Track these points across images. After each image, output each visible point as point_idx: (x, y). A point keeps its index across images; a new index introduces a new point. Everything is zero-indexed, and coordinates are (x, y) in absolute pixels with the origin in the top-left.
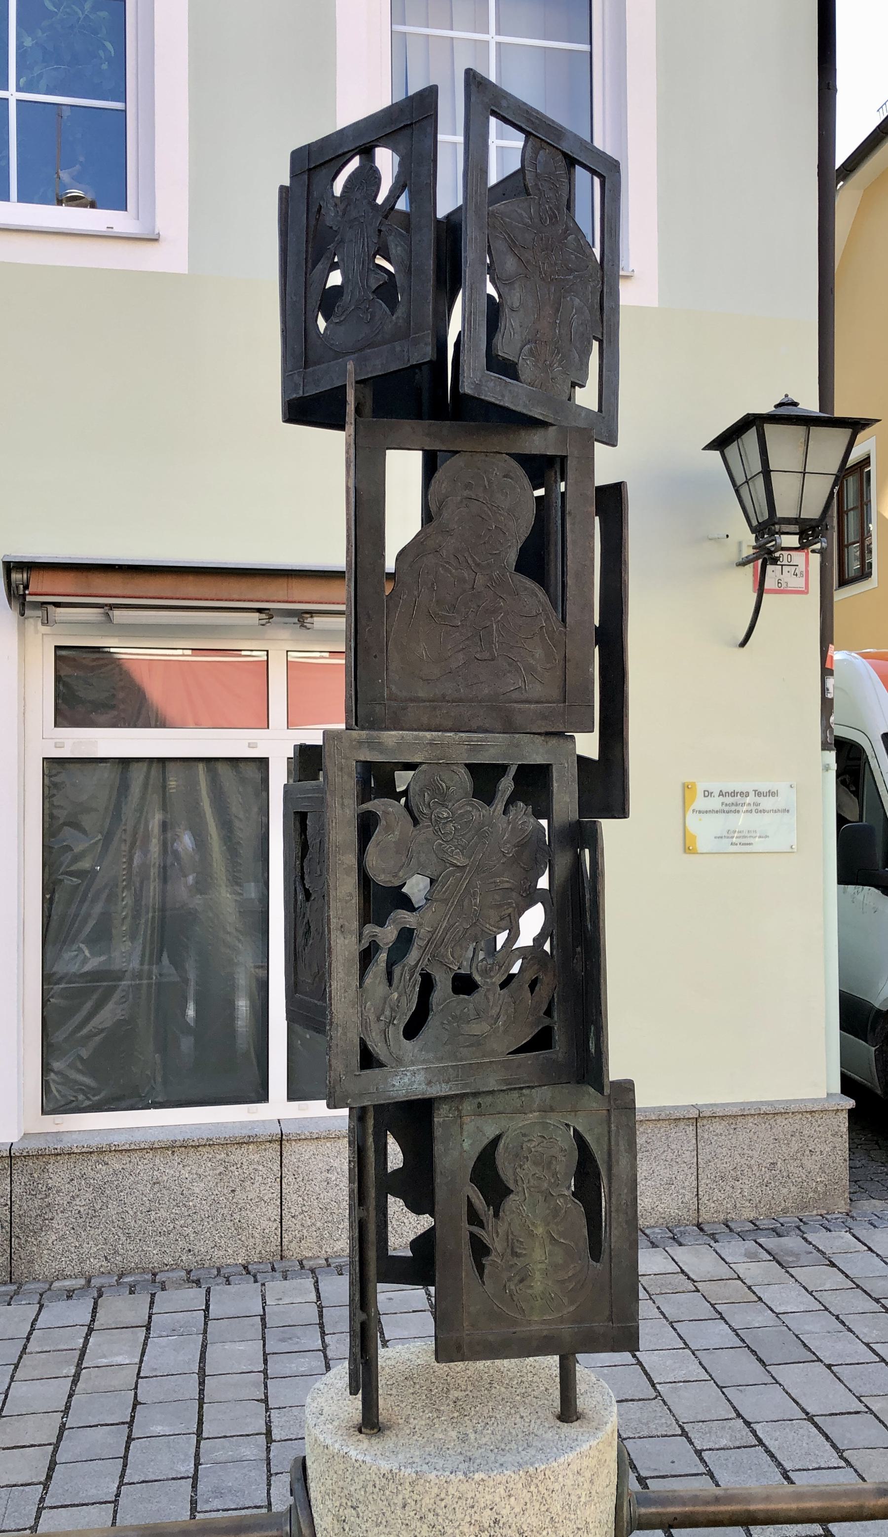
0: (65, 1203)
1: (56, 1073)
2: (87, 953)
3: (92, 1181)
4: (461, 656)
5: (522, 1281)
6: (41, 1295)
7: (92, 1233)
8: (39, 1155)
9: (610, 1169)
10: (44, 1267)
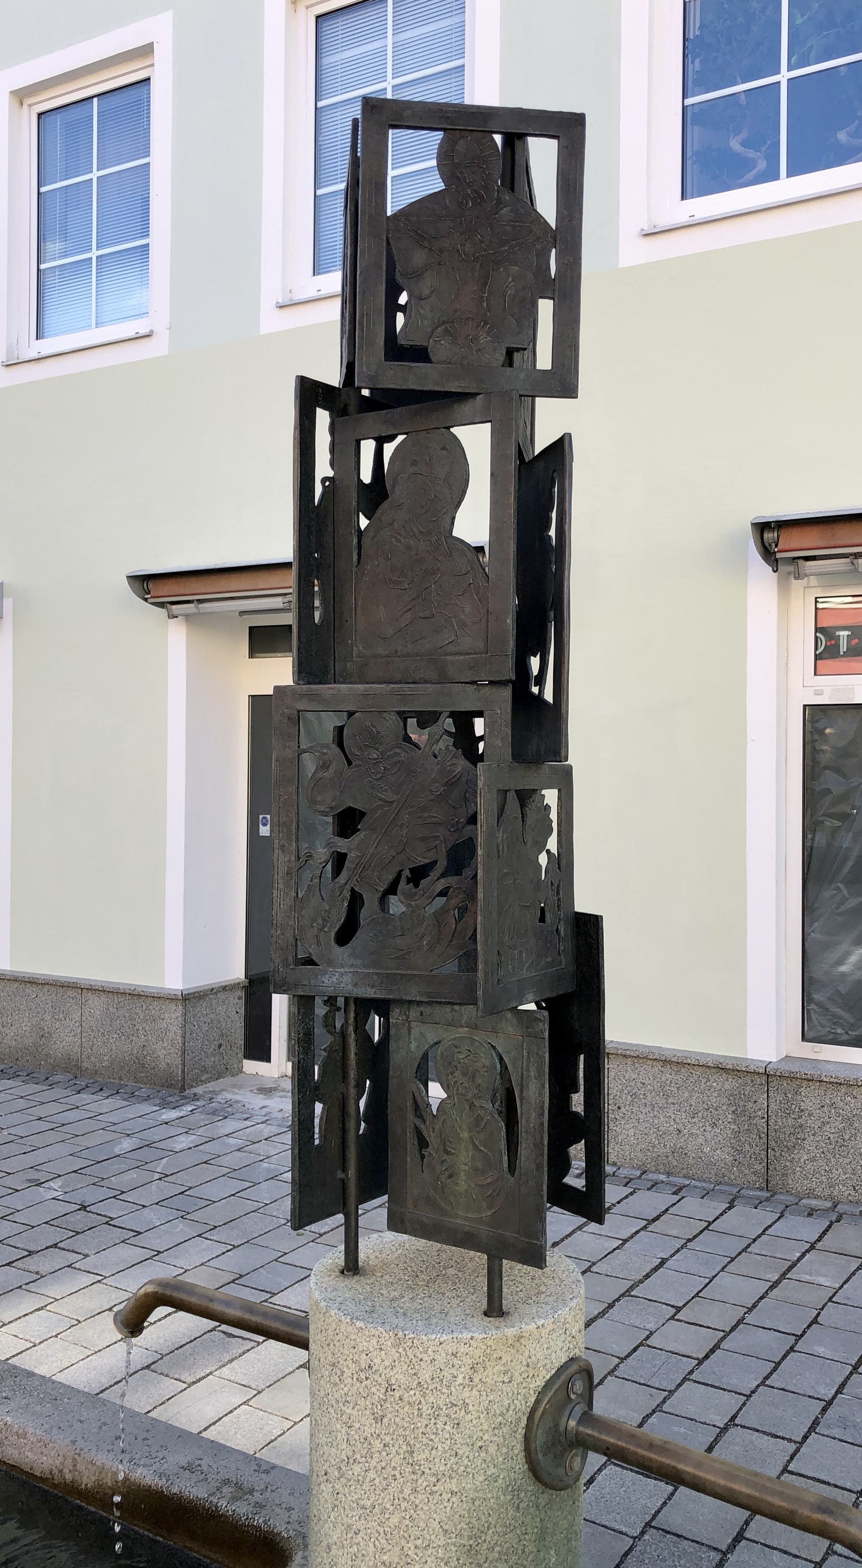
0: (816, 1127)
1: (816, 1004)
2: (845, 892)
3: (841, 1111)
4: (408, 615)
5: (450, 1176)
6: (787, 1207)
7: (841, 1160)
8: (792, 1077)
9: (521, 1092)
10: (796, 1183)
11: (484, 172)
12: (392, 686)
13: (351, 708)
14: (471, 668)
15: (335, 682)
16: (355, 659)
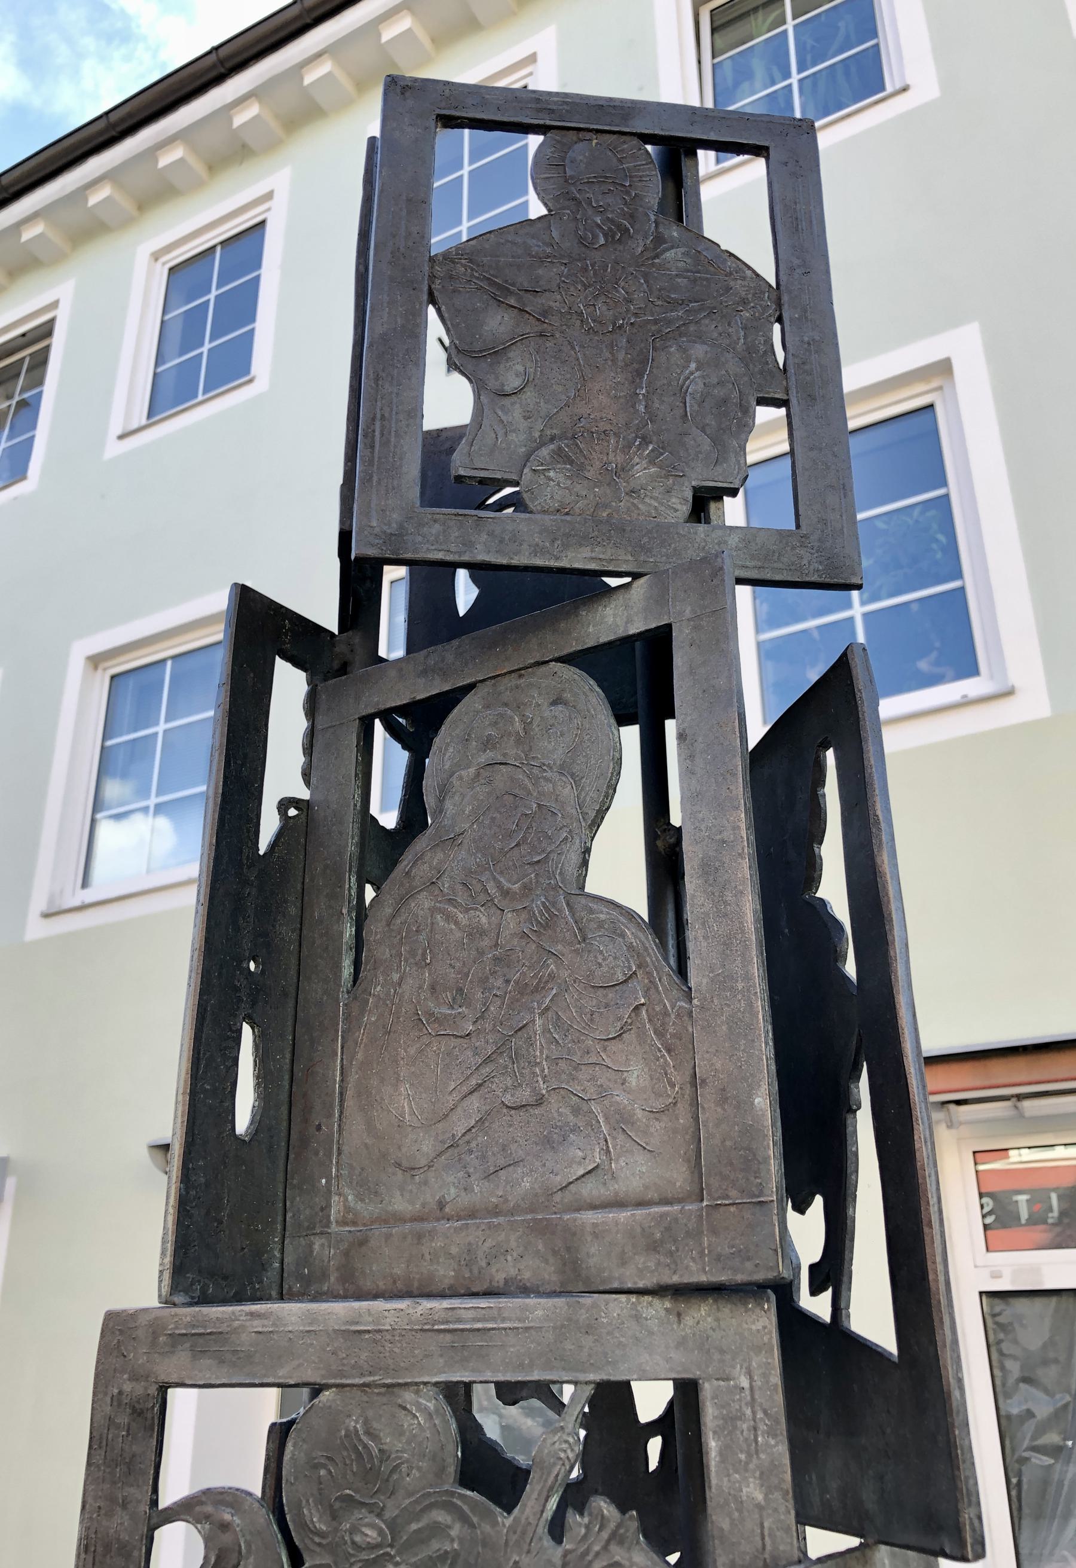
4: (475, 1103)
11: (628, 193)
12: (427, 1304)
13: (313, 1376)
14: (653, 1247)
15: (281, 1298)
16: (334, 1228)
